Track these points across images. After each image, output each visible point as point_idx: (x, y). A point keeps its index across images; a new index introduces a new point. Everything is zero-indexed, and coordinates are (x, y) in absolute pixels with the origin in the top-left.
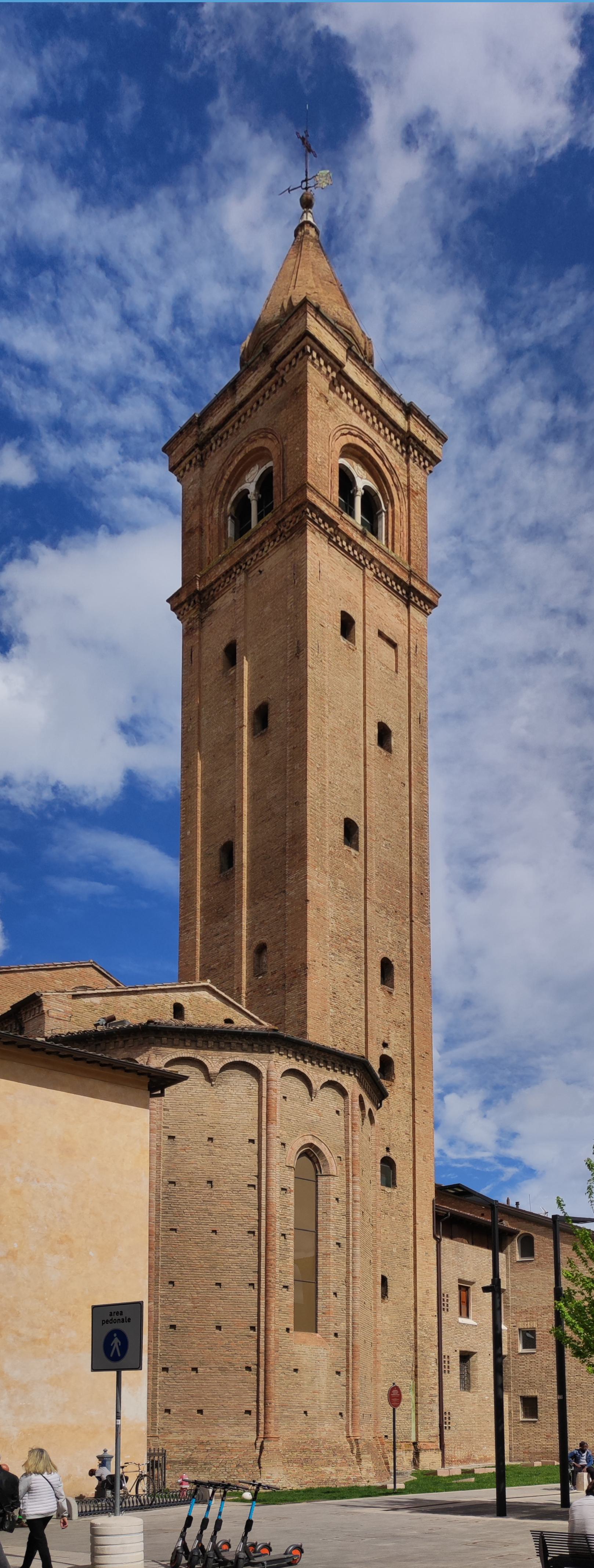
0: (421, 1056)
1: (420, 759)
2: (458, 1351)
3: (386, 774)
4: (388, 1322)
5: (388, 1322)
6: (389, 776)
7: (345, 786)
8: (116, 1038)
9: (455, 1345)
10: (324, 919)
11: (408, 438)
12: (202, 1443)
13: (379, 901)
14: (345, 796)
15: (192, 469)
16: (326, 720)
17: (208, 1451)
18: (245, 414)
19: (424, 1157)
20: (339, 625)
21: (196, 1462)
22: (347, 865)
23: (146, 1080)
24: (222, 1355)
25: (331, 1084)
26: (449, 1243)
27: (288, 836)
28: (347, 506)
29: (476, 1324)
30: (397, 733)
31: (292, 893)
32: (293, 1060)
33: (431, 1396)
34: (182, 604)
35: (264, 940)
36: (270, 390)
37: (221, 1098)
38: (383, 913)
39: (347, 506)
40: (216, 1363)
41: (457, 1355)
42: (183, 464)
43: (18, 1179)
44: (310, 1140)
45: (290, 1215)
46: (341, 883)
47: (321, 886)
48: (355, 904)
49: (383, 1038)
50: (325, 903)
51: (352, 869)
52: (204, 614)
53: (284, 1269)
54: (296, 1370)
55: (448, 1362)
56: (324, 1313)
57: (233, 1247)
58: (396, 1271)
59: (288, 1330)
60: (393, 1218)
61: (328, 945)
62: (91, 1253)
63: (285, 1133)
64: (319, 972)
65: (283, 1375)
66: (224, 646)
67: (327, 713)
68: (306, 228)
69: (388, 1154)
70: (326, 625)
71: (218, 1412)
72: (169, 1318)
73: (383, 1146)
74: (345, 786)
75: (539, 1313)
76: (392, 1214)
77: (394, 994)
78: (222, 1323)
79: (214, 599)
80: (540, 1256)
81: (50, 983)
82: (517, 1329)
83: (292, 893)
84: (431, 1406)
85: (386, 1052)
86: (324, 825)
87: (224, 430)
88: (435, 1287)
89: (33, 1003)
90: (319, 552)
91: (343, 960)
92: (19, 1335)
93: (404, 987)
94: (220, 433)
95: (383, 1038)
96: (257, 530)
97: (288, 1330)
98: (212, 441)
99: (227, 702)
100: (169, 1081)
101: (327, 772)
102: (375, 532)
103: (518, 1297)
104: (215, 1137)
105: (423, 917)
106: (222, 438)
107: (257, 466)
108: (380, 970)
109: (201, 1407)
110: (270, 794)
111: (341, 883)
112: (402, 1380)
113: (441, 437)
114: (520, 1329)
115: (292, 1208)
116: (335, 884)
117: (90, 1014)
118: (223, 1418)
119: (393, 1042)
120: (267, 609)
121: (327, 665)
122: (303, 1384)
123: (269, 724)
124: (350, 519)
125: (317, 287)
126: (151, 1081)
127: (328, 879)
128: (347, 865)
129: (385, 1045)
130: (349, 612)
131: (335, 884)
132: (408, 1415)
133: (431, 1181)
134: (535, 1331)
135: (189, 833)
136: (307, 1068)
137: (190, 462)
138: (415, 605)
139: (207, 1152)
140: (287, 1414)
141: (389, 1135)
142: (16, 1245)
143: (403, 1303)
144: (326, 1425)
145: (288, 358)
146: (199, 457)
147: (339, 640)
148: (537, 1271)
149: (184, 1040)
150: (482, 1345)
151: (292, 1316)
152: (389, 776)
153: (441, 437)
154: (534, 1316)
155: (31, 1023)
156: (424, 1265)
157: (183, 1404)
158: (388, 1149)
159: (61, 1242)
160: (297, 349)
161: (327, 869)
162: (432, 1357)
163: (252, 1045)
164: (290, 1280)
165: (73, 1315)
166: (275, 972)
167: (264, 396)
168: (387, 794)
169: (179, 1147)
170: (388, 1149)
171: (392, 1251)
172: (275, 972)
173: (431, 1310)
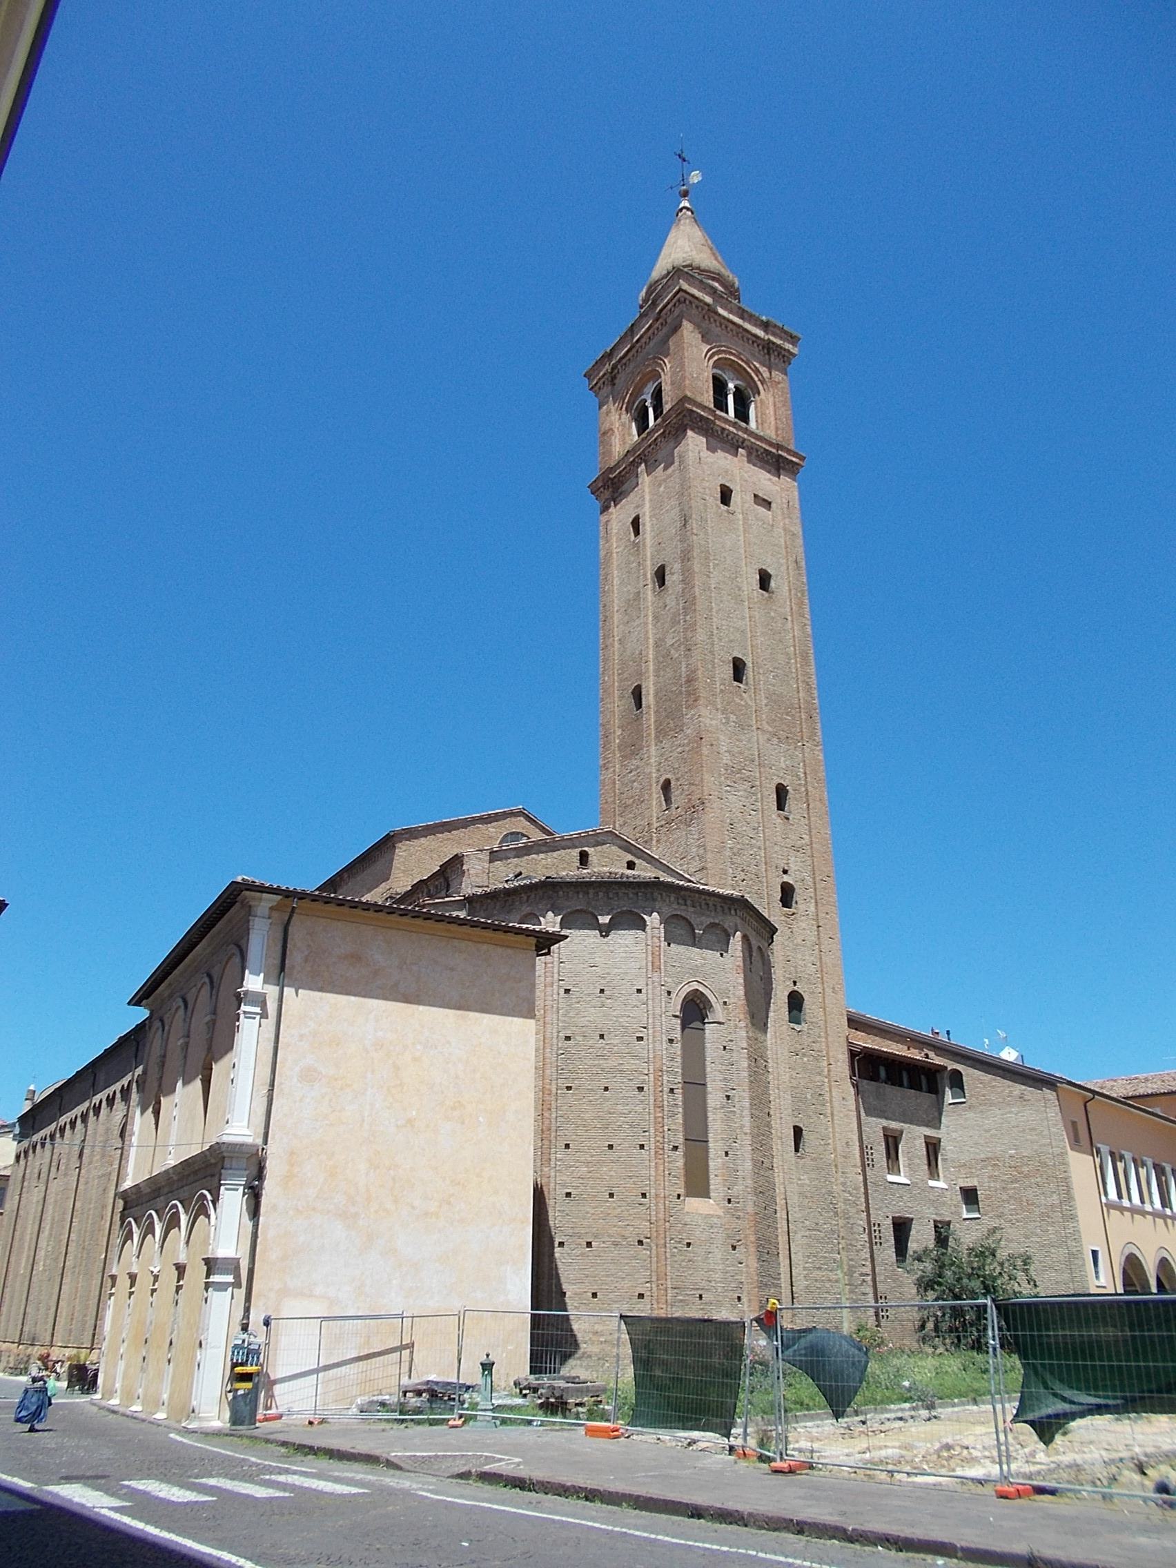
0: (822, 880)
1: (799, 595)
2: (891, 1217)
3: (769, 613)
4: (807, 1182)
5: (807, 1182)
6: (772, 614)
7: (731, 630)
8: (521, 894)
9: (885, 1210)
10: (718, 753)
11: (768, 344)
12: (596, 1333)
13: (770, 729)
14: (732, 638)
15: (605, 388)
16: (712, 576)
17: (602, 1342)
18: (641, 347)
19: (834, 988)
20: (719, 495)
21: (590, 1356)
22: (737, 700)
23: (533, 941)
24: (615, 1226)
25: (713, 925)
26: (868, 1084)
27: (684, 680)
28: (721, 404)
29: (909, 1182)
30: (777, 576)
31: (689, 731)
32: (675, 906)
33: (862, 1275)
34: (599, 488)
35: (669, 776)
36: (658, 328)
37: (611, 948)
38: (775, 741)
39: (721, 404)
40: (609, 1236)
41: (889, 1221)
42: (599, 385)
43: (419, 1047)
44: (695, 986)
45: (677, 1067)
46: (733, 717)
47: (714, 722)
48: (747, 736)
49: (782, 865)
50: (718, 738)
51: (742, 703)
52: (616, 495)
53: (673, 1127)
54: (689, 1245)
55: (879, 1231)
56: (716, 1176)
57: (623, 1104)
58: (812, 1121)
59: (679, 1196)
60: (805, 1059)
61: (723, 778)
62: (481, 1119)
63: (670, 980)
64: (714, 805)
65: (675, 1250)
66: (631, 520)
67: (712, 570)
68: (684, 211)
69: (796, 988)
70: (707, 498)
71: (611, 1296)
72: (564, 1186)
73: (790, 979)
74: (731, 630)
75: (979, 1167)
76: (804, 1055)
77: (791, 818)
78: (614, 1190)
79: (623, 483)
80: (972, 1096)
81: (485, 832)
82: (958, 1188)
83: (689, 731)
84: (863, 1289)
85: (786, 878)
86: (714, 667)
87: (627, 358)
88: (856, 1137)
89: (456, 862)
90: (699, 443)
91: (738, 791)
92: (413, 1208)
93: (800, 811)
94: (624, 361)
95: (782, 865)
96: (654, 431)
97: (679, 1196)
98: (619, 367)
99: (634, 564)
100: (553, 941)
101: (715, 620)
102: (746, 420)
103: (955, 1147)
104: (605, 989)
105: (814, 740)
106: (625, 364)
107: (651, 383)
108: (775, 797)
109: (595, 1289)
110: (669, 642)
111: (733, 717)
112: (826, 1255)
113: (794, 339)
114: (961, 1188)
115: (679, 1059)
116: (727, 719)
117: (505, 868)
118: (616, 1302)
119: (793, 868)
120: (662, 489)
121: (710, 530)
122: (696, 1260)
123: (666, 583)
124: (723, 414)
125: (692, 250)
126: (538, 941)
127: (720, 716)
128: (737, 700)
129: (785, 872)
130: (727, 484)
131: (727, 719)
132: (837, 1299)
133: (842, 1015)
134: (976, 1190)
135: (606, 678)
136: (689, 913)
137: (604, 383)
138: (784, 469)
139: (599, 1004)
140: (681, 1298)
141: (796, 967)
142: (414, 1113)
143: (822, 1159)
144: (724, 1312)
145: (669, 307)
146: (610, 379)
147: (720, 508)
148: (970, 1115)
149: (578, 893)
150: (919, 1208)
151: (682, 1179)
152: (772, 614)
153: (794, 339)
154: (974, 1170)
155: (454, 881)
156: (841, 1112)
157: (578, 1286)
158: (795, 983)
159: (454, 1109)
160: (674, 301)
161: (719, 706)
162: (860, 1225)
163: (637, 894)
164: (680, 1139)
165: (463, 1184)
166: (678, 808)
167: (654, 333)
168: (771, 630)
169: (574, 1000)
170: (795, 983)
171: (806, 1097)
172: (678, 808)
173: (855, 1166)
